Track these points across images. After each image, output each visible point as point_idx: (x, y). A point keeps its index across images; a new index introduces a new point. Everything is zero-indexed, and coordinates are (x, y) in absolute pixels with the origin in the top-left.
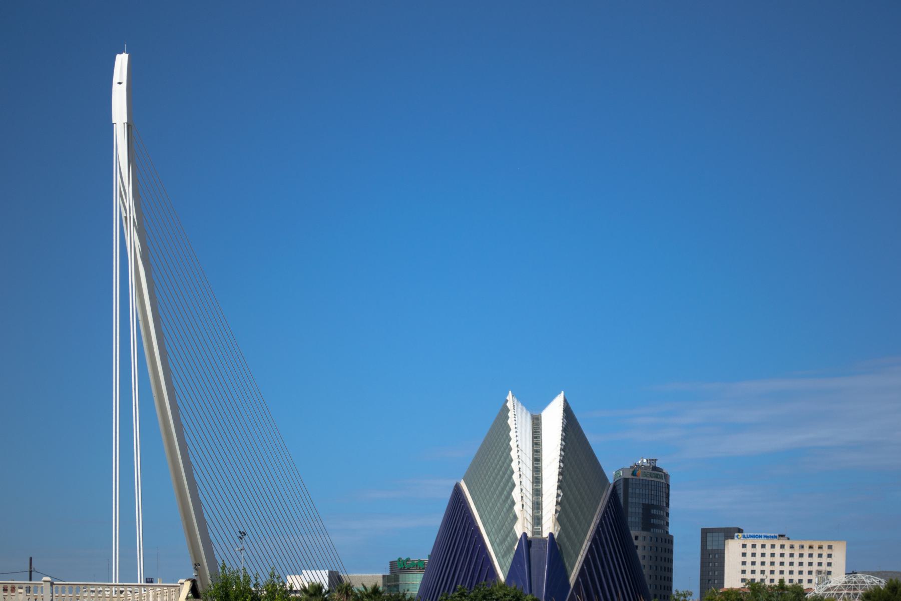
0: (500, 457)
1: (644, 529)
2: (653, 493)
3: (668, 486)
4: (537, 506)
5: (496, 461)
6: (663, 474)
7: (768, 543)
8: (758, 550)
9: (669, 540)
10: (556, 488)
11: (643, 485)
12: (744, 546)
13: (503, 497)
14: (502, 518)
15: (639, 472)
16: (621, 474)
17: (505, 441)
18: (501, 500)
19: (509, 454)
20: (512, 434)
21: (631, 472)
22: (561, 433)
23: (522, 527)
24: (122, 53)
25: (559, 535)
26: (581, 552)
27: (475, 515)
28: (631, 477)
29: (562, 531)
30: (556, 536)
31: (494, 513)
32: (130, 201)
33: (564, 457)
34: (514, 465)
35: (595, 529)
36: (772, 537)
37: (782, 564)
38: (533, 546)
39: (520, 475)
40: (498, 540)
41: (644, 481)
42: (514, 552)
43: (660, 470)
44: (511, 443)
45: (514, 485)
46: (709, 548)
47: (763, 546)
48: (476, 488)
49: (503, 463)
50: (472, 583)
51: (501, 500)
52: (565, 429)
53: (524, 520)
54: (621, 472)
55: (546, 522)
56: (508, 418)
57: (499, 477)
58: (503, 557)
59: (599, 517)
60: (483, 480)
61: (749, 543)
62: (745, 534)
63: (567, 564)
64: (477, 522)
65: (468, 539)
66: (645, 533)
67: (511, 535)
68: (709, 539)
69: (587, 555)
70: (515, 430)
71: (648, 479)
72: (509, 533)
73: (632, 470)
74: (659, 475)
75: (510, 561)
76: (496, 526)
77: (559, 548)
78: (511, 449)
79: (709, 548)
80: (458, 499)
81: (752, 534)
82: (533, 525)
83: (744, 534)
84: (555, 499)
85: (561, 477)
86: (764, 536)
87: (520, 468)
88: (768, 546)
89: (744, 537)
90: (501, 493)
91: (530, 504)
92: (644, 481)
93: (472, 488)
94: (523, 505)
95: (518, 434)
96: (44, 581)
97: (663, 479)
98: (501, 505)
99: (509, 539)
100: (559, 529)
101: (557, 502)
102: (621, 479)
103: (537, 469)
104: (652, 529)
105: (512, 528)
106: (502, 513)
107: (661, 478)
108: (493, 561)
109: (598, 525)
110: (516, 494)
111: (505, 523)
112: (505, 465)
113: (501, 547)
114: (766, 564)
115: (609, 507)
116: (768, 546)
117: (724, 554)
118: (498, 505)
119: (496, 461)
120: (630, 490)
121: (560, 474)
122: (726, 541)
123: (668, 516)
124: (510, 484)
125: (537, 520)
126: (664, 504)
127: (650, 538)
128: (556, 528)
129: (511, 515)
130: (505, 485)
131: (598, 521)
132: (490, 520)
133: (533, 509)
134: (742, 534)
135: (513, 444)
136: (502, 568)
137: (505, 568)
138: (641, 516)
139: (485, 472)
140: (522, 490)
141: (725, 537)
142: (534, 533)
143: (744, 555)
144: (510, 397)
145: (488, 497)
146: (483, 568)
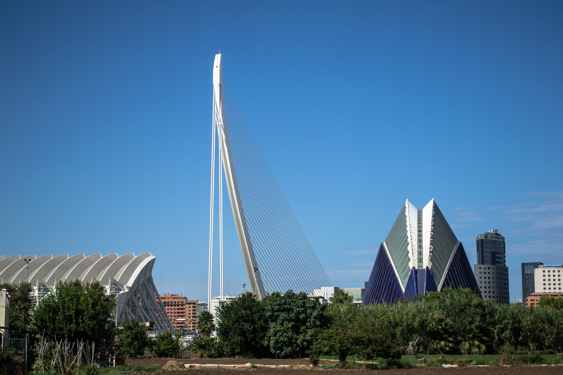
0: (402, 230)
1: (492, 264)
2: (496, 246)
3: (504, 243)
4: (420, 253)
5: (400, 232)
6: (501, 237)
7: (556, 270)
8: (552, 273)
9: (507, 269)
10: (430, 244)
11: (491, 242)
12: (544, 271)
13: (403, 249)
14: (403, 259)
15: (489, 236)
16: (480, 237)
17: (404, 222)
18: (402, 251)
19: (406, 229)
20: (407, 219)
21: (484, 236)
22: (431, 218)
23: (413, 264)
24: (218, 54)
25: (431, 267)
26: (443, 276)
27: (390, 258)
28: (484, 238)
29: (433, 266)
30: (430, 268)
31: (399, 257)
32: (220, 117)
33: (433, 229)
34: (408, 234)
35: (450, 264)
36: (558, 267)
37: (549, 280)
38: (418, 273)
39: (411, 239)
40: (401, 270)
41: (490, 241)
42: (409, 276)
43: (500, 235)
44: (407, 223)
45: (408, 244)
46: (526, 273)
47: (554, 271)
48: (390, 246)
49: (403, 233)
50: (388, 291)
51: (402, 251)
52: (434, 216)
53: (414, 260)
54: (479, 236)
55: (424, 261)
56: (405, 211)
57: (401, 240)
58: (404, 279)
59: (452, 258)
60: (393, 241)
61: (547, 270)
62: (544, 266)
63: (436, 282)
64: (390, 262)
65: (387, 270)
66: (493, 266)
67: (407, 267)
68: (526, 268)
69: (446, 277)
70: (409, 217)
71: (493, 239)
72: (406, 267)
73: (485, 235)
74: (499, 237)
75: (407, 280)
76: (400, 263)
77: (431, 274)
78: (406, 226)
79: (526, 273)
80: (382, 251)
81: (548, 265)
82: (418, 263)
83: (543, 265)
84: (429, 250)
85: (432, 239)
86: (554, 267)
87: (411, 235)
88: (556, 271)
89: (543, 267)
90: (402, 248)
91: (417, 253)
92: (490, 241)
93: (388, 245)
94: (413, 253)
95: (410, 219)
96: (3, 291)
97: (501, 239)
98: (402, 253)
99: (406, 270)
100: (431, 264)
101: (430, 251)
102: (479, 240)
103: (420, 235)
104: (497, 264)
105: (408, 264)
106: (403, 257)
107: (500, 239)
108: (399, 281)
109: (452, 262)
110: (409, 248)
111: (404, 262)
112: (404, 234)
113: (402, 274)
114: (556, 280)
115: (457, 253)
116: (556, 271)
117: (534, 275)
118: (401, 253)
119: (400, 232)
120: (484, 245)
121: (431, 237)
122: (535, 269)
123: (505, 257)
124: (406, 243)
125: (420, 260)
126: (502, 252)
127: (496, 268)
128: (430, 264)
129: (407, 258)
130: (404, 244)
131: (452, 260)
132: (397, 261)
133: (418, 255)
134: (543, 265)
135: (408, 224)
136: (403, 284)
137: (404, 284)
138: (490, 257)
139: (394, 238)
140: (412, 246)
141: (534, 267)
142: (419, 267)
143: (544, 276)
144: (407, 202)
145: (396, 249)
146: (394, 284)
